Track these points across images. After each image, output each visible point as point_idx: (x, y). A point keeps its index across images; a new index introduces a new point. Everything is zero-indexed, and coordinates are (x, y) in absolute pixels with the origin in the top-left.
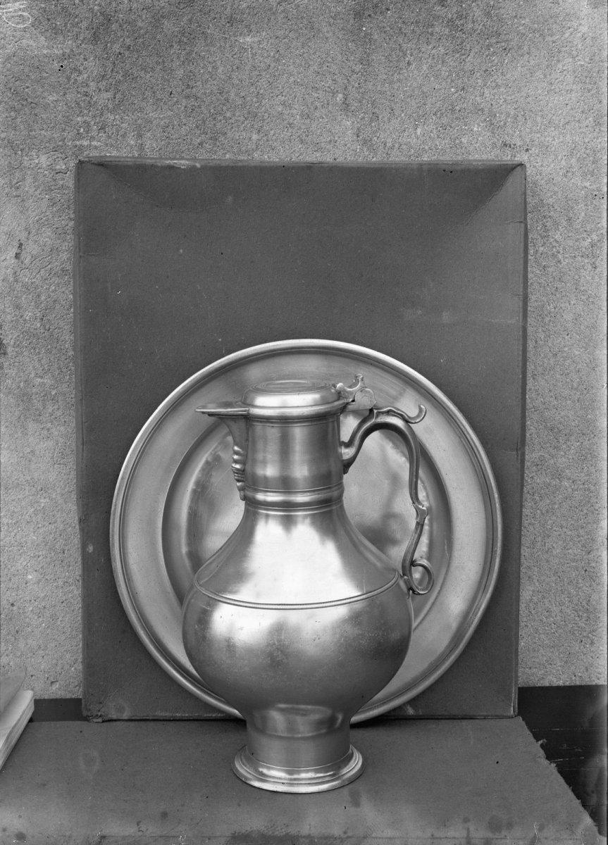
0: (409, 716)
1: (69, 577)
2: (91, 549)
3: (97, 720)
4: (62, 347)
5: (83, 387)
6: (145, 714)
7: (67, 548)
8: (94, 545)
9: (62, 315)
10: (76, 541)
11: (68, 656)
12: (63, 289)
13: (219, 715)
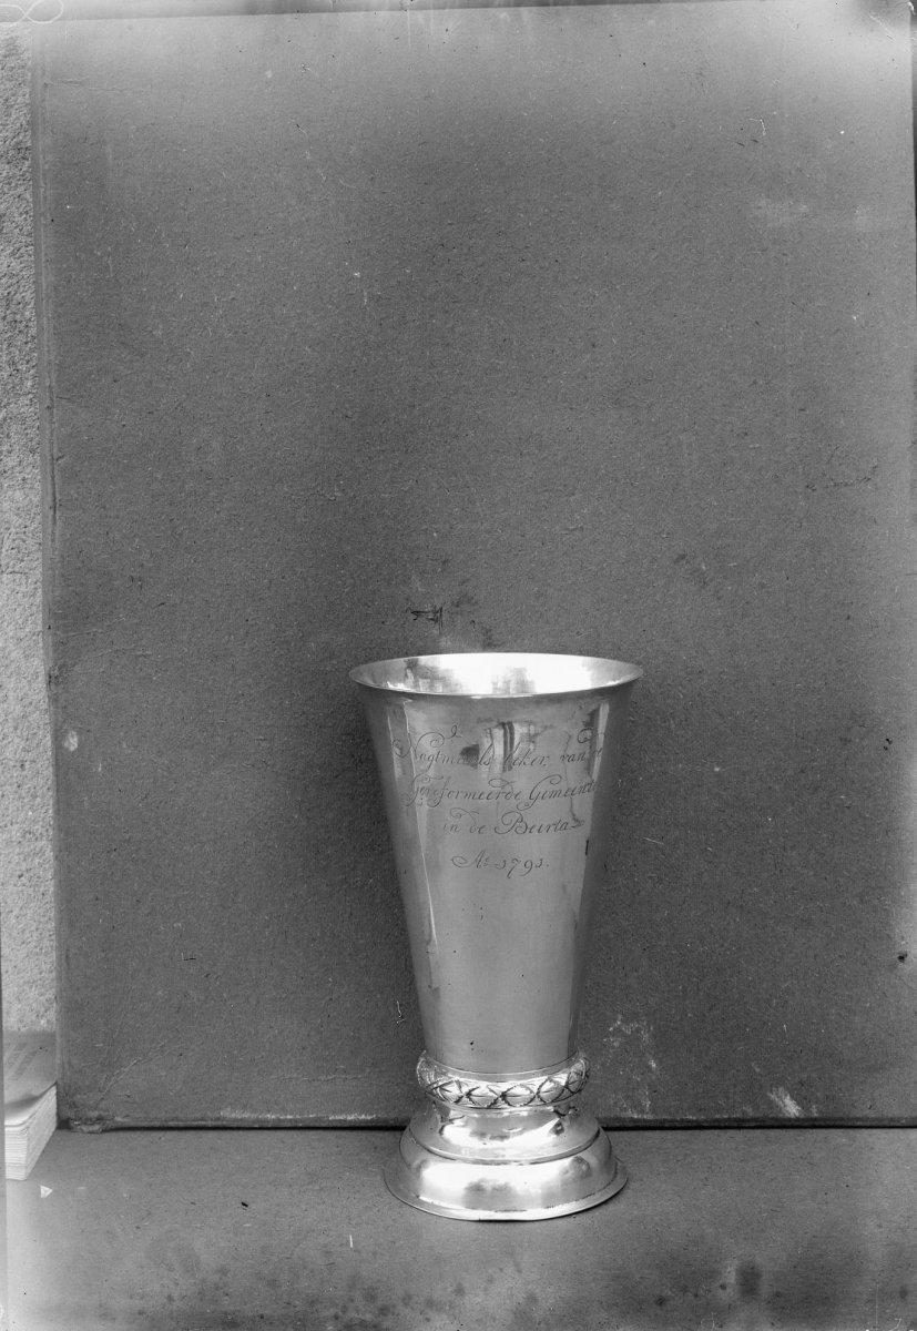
0: (790, 1119)
1: (35, 822)
2: (73, 742)
3: (91, 1128)
4: (18, 317)
5: (54, 376)
6: (198, 1115)
7: (30, 756)
8: (79, 733)
9: (17, 245)
10: (40, 719)
11: (33, 993)
12: (20, 190)
13: (363, 1117)
